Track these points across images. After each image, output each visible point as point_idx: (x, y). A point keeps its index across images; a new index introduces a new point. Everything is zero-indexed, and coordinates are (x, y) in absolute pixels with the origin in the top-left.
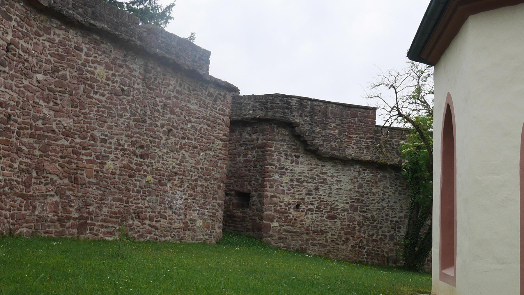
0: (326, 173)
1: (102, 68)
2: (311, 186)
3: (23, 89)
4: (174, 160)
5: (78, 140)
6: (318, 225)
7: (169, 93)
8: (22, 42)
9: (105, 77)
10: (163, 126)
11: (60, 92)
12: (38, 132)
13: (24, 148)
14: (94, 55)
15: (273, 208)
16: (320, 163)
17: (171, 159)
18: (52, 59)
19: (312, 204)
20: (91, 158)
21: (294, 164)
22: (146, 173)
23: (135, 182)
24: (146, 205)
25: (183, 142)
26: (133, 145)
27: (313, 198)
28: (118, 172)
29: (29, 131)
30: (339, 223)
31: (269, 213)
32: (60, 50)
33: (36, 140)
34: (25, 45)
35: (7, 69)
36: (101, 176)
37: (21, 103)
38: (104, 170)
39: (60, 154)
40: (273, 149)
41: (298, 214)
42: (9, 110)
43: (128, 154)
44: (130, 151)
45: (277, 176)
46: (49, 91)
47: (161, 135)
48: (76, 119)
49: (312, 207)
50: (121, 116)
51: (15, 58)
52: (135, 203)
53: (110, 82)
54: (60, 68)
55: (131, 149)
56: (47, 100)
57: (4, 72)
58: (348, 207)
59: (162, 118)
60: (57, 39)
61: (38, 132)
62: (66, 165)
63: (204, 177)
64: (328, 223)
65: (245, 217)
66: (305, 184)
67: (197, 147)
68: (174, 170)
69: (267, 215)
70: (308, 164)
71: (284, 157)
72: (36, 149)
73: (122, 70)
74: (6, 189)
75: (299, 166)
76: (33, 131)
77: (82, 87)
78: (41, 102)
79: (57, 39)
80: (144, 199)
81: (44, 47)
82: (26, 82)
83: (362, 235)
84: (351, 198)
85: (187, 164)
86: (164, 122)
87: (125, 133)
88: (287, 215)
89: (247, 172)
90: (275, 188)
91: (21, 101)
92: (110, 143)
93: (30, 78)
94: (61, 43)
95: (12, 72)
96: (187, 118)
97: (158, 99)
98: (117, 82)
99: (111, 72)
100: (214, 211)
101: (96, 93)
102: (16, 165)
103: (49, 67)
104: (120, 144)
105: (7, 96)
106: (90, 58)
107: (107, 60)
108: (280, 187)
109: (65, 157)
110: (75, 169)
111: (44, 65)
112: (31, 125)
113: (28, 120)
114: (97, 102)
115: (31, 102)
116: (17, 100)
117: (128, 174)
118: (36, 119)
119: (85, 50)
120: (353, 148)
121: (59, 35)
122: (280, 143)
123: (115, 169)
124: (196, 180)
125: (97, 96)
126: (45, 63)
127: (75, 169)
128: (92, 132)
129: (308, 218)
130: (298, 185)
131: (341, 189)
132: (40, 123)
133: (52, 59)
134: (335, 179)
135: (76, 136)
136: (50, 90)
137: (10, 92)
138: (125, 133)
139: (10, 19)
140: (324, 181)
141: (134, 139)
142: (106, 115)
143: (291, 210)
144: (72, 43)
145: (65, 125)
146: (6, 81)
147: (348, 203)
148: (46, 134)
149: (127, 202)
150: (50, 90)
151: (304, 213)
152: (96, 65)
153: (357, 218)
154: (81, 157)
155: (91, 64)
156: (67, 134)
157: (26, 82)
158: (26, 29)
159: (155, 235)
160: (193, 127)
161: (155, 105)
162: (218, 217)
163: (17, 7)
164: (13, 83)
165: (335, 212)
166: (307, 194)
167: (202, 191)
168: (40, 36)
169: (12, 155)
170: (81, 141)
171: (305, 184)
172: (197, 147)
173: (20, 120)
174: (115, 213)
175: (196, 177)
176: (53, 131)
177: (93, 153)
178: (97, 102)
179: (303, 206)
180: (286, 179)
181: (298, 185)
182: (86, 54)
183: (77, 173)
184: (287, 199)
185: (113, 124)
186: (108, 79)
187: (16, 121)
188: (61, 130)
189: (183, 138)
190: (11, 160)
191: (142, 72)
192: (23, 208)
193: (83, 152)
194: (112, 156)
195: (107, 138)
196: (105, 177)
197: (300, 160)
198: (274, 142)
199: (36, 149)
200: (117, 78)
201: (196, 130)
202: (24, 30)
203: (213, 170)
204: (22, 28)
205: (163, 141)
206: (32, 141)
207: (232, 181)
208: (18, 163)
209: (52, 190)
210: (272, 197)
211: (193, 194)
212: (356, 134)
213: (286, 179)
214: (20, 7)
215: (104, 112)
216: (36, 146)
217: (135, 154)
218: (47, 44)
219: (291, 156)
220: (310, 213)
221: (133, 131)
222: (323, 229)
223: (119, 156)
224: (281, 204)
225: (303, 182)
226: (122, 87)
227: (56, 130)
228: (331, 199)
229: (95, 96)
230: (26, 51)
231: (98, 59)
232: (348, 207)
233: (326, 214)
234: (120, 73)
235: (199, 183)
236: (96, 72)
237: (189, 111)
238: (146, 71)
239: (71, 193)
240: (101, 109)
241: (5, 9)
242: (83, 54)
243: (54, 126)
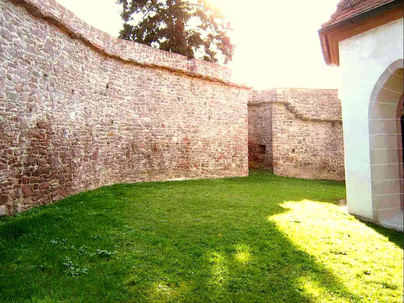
0: (309, 130)
1: (165, 88)
2: (301, 138)
3: (119, 106)
4: (214, 132)
5: (154, 128)
6: (306, 160)
7: (207, 95)
8: (115, 81)
9: (167, 92)
10: (205, 114)
11: (141, 104)
12: (131, 127)
13: (123, 136)
14: (159, 81)
15: (278, 153)
16: (305, 124)
17: (212, 132)
18: (135, 87)
19: (302, 149)
20: (163, 137)
21: (289, 127)
22: (197, 141)
23: (191, 147)
24: (199, 158)
25: (219, 121)
26: (188, 127)
27: (302, 145)
28: (180, 142)
29: (126, 127)
30: (319, 158)
31: (276, 155)
32: (139, 82)
33: (130, 131)
34: (118, 83)
35: (108, 97)
36: (170, 146)
37: (119, 113)
38: (172, 142)
39: (145, 137)
40: (276, 119)
41: (294, 155)
42: (112, 118)
43: (185, 132)
44: (186, 130)
45: (279, 135)
46: (135, 104)
47: (205, 119)
48: (152, 117)
49: (302, 150)
50: (179, 112)
51: (112, 91)
52: (192, 158)
53: (170, 95)
54: (140, 92)
55: (187, 129)
56: (134, 109)
57: (107, 99)
58: (324, 148)
59: (204, 110)
60: (136, 76)
61: (131, 127)
62: (149, 142)
63: (234, 139)
64: (312, 158)
65: (264, 159)
66: (297, 137)
67: (228, 123)
68: (214, 138)
69: (275, 157)
70: (298, 126)
71: (283, 123)
72: (130, 136)
73: (177, 87)
74: (115, 159)
75: (293, 127)
76: (128, 127)
77: (154, 100)
78: (131, 111)
79: (136, 76)
80: (198, 155)
81: (129, 82)
82: (120, 102)
83: (334, 164)
84: (325, 143)
85: (223, 134)
86: (205, 112)
87: (182, 121)
88: (287, 156)
89: (263, 134)
90: (279, 141)
91: (118, 112)
92: (174, 127)
93: (123, 99)
94: (139, 78)
95: (112, 98)
96: (220, 108)
97: (201, 100)
98: (174, 94)
99: (170, 89)
100: (242, 158)
101: (162, 102)
102: (119, 146)
103: (134, 91)
104: (179, 127)
105: (110, 111)
106: (157, 84)
107: (167, 83)
108: (282, 141)
109: (148, 138)
110: (154, 144)
111: (130, 91)
112: (126, 124)
113: (125, 122)
114: (164, 106)
115: (125, 112)
116: (116, 112)
117: (186, 143)
118: (128, 120)
119: (154, 80)
120: (325, 114)
121: (137, 74)
122: (280, 115)
123: (178, 141)
124: (229, 142)
125: (164, 103)
126: (131, 90)
127: (154, 144)
128: (162, 123)
129: (300, 157)
130: (292, 138)
131: (318, 138)
132: (131, 123)
133: (135, 87)
134: (314, 133)
135: (153, 126)
136: (135, 104)
137: (111, 108)
138: (182, 121)
139: (107, 71)
140: (308, 135)
141: (187, 124)
142: (170, 113)
143: (290, 153)
144: (146, 77)
145: (146, 121)
146: (108, 103)
147: (324, 146)
148: (136, 127)
149: (188, 158)
150: (135, 104)
151: (297, 154)
152: (161, 87)
153: (330, 153)
154: (157, 137)
155: (158, 87)
156: (147, 126)
157: (120, 102)
158: (118, 74)
159: (206, 174)
160: (224, 112)
161: (199, 103)
162: (245, 161)
163: (110, 64)
164: (113, 103)
165: (316, 152)
166: (298, 143)
167: (233, 147)
168: (126, 76)
169: (116, 141)
170: (156, 128)
171: (297, 137)
172: (228, 123)
173: (119, 122)
174: (180, 165)
175: (229, 140)
176: (140, 125)
177: (164, 134)
178: (164, 106)
179: (296, 150)
180: (285, 135)
181: (292, 138)
182: (155, 82)
183: (156, 146)
184: (287, 147)
185: (175, 117)
186: (169, 93)
187: (116, 123)
188: (144, 124)
189: (219, 119)
190: (116, 144)
191: (189, 86)
192: (127, 168)
193: (158, 134)
194: (175, 134)
195: (171, 125)
196: (172, 146)
197: (292, 124)
198: (276, 115)
199: (130, 136)
200: (174, 92)
201: (226, 114)
202: (116, 75)
203: (239, 135)
204: (115, 74)
205: (206, 123)
206: (128, 132)
207: (256, 139)
208: (121, 144)
209: (142, 157)
210: (277, 146)
211: (228, 149)
212: (326, 105)
213: (285, 135)
214: (112, 64)
215: (168, 111)
216: (131, 134)
217: (189, 131)
218: (131, 80)
219: (287, 122)
220: (301, 153)
221: (187, 119)
222: (310, 162)
223: (180, 134)
224: (283, 150)
225: (295, 137)
226: (178, 96)
227: (141, 124)
228: (313, 145)
229: (162, 104)
230: (120, 86)
231: (162, 83)
232: (324, 148)
233: (311, 154)
234: (176, 89)
235: (231, 143)
236: (161, 90)
237: (221, 104)
238: (192, 85)
239: (154, 156)
240: (167, 110)
241: (103, 66)
242: (152, 82)
243: (140, 123)
